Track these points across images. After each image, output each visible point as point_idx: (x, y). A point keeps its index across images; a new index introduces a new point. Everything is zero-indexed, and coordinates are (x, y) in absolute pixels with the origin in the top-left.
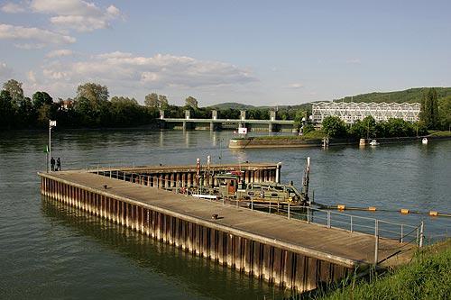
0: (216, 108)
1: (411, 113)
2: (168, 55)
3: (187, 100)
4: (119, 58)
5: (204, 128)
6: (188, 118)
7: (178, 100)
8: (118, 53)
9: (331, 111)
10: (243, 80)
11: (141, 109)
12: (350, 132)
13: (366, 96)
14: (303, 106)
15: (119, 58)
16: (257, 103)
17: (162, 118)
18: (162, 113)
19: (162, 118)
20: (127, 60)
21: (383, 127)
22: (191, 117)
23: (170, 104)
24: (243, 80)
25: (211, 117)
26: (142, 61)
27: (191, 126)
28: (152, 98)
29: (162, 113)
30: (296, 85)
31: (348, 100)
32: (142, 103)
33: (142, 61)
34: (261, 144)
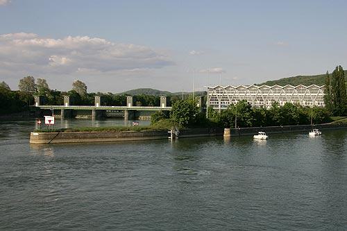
0: (99, 94)
1: (313, 99)
2: (78, 37)
3: (74, 84)
4: (25, 38)
5: (86, 117)
6: (67, 105)
7: (63, 85)
8: (23, 34)
9: (240, 96)
10: (163, 64)
11: (17, 94)
12: (312, 115)
13: (293, 79)
14: (198, 94)
15: (25, 38)
16: (116, 90)
17: (37, 105)
18: (37, 98)
19: (37, 105)
20: (33, 41)
21: (263, 113)
22: (71, 104)
23: (51, 88)
24: (163, 64)
25: (125, 104)
26: (51, 43)
27: (102, 116)
28: (28, 82)
29: (37, 98)
30: (216, 70)
31: (270, 83)
32: (14, 86)
33: (51, 43)
34: (76, 137)
